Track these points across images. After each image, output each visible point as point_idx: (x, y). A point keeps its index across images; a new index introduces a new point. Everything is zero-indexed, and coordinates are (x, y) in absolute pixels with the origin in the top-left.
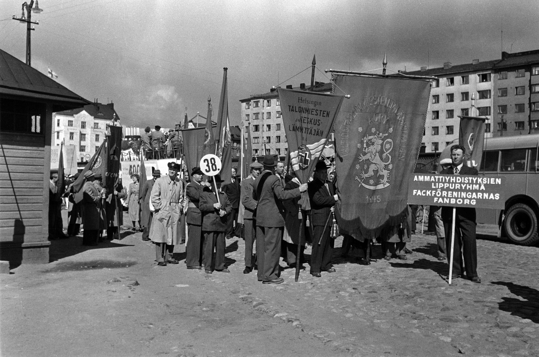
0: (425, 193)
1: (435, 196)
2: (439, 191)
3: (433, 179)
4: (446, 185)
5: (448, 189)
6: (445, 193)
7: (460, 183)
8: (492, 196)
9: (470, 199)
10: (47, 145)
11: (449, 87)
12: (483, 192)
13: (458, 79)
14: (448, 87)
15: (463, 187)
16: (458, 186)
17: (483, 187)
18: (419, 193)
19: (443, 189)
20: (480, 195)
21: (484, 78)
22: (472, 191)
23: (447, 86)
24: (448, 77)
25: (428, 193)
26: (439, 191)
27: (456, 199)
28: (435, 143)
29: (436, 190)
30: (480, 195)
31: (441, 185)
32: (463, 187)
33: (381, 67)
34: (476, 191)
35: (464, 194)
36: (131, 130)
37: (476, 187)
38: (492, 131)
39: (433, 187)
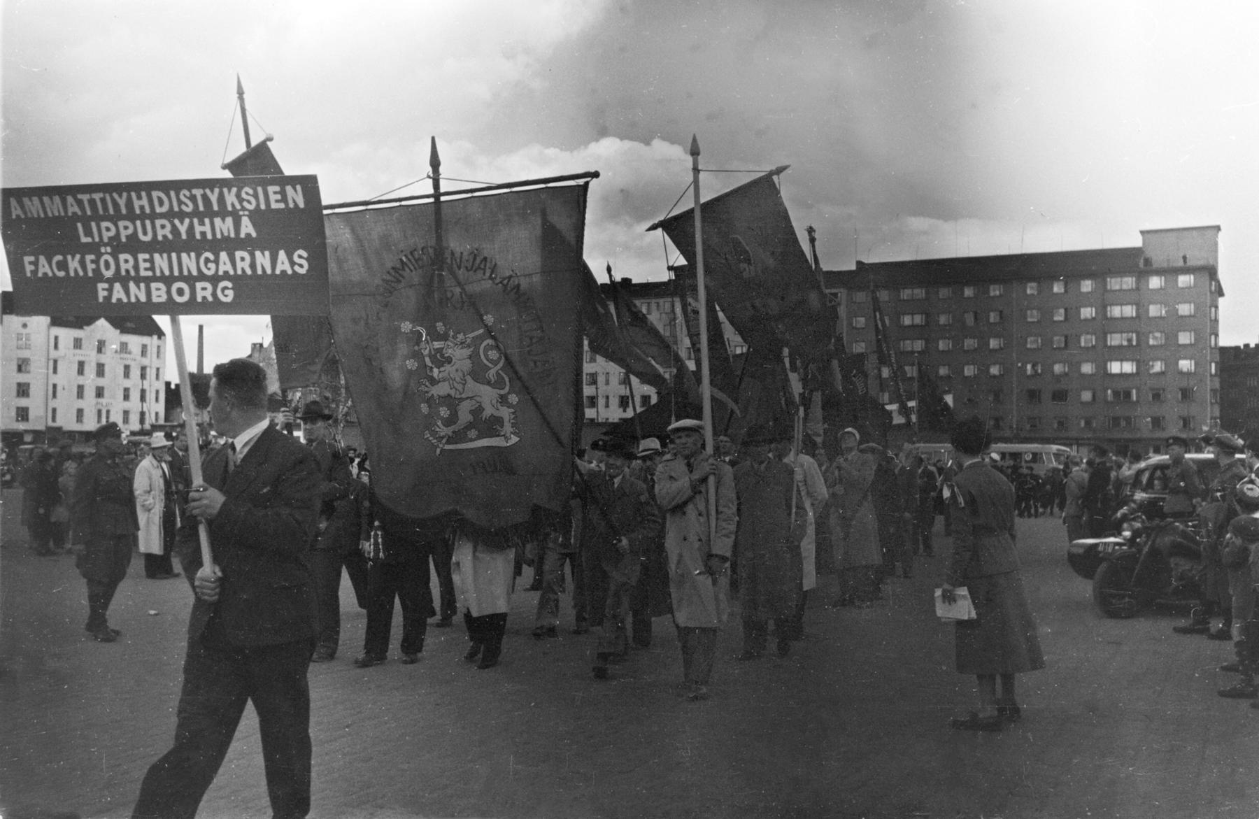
0: (63, 266)
1: (98, 277)
5: (133, 245)
8: (283, 264)
12: (248, 244)
17: (247, 228)
22: (155, 246)
25: (74, 264)
27: (168, 280)
29: (94, 248)
31: (107, 230)
34: (231, 244)
35: (189, 262)
37: (225, 227)
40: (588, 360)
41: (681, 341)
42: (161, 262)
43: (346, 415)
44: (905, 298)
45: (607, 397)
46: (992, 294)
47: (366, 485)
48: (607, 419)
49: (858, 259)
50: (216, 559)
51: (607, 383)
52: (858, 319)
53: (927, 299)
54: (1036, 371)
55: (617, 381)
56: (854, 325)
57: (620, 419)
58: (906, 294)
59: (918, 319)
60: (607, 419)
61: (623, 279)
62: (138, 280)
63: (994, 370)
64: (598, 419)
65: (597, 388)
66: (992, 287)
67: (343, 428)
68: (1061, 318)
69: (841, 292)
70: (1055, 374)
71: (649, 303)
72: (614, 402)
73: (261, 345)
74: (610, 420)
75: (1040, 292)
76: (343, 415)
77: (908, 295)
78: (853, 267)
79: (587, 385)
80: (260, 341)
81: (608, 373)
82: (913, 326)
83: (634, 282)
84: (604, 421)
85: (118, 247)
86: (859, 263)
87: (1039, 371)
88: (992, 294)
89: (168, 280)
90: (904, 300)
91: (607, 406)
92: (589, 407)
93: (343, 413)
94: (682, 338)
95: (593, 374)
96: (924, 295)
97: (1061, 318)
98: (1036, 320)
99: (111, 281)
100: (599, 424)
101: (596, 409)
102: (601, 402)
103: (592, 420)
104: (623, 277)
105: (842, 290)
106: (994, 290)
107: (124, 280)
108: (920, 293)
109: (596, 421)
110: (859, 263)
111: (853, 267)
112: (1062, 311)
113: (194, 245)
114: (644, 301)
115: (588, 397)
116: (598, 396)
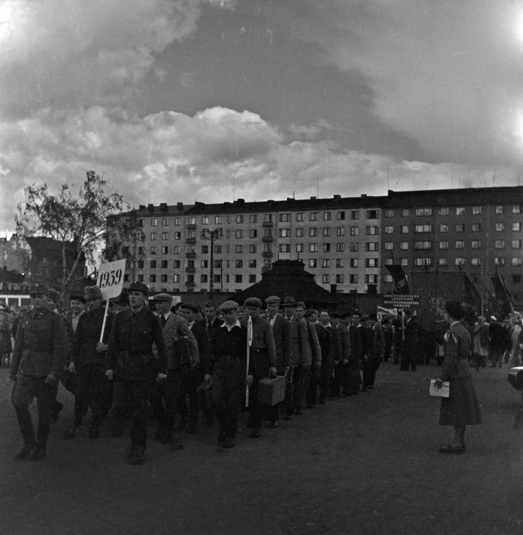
0: (389, 302)
1: (393, 303)
2: (395, 301)
3: (391, 296)
4: (398, 299)
5: (398, 300)
6: (397, 302)
7: (403, 297)
8: (416, 303)
9: (408, 305)
10: (176, 206)
11: (341, 221)
12: (412, 301)
13: (348, 213)
14: (339, 221)
15: (404, 299)
16: (402, 299)
17: (412, 299)
18: (387, 302)
19: (396, 300)
20: (411, 303)
21: (373, 215)
22: (401, 301)
23: (338, 220)
24: (338, 211)
25: (391, 302)
26: (395, 301)
27: (402, 304)
28: (255, 265)
29: (394, 300)
30: (411, 303)
31: (395, 299)
32: (404, 299)
33: (10, 230)
34: (410, 301)
35: (405, 303)
36: (178, 223)
37: (409, 299)
38: (380, 266)
39: (392, 299)
40: (216, 252)
41: (276, 240)
42: (401, 302)
43: (66, 286)
44: (419, 215)
45: (228, 276)
46: (474, 213)
47: (330, 327)
48: (228, 290)
49: (390, 189)
50: (405, 336)
51: (228, 266)
52: (389, 227)
53: (433, 215)
54: (501, 263)
55: (234, 265)
56: (386, 231)
57: (236, 290)
58: (419, 212)
59: (427, 228)
60: (228, 290)
61: (239, 200)
62: (398, 304)
63: (475, 262)
64: (222, 290)
65: (222, 270)
66: (474, 208)
67: (65, 294)
68: (518, 229)
69: (378, 211)
70: (513, 264)
71: (255, 216)
72: (232, 279)
73: (5, 239)
74: (230, 291)
75: (504, 212)
76: (65, 286)
77: (420, 213)
78: (386, 194)
79: (215, 267)
80: (5, 237)
81: (228, 260)
82: (424, 233)
83: (246, 201)
84: (226, 291)
85: (396, 300)
86: (390, 192)
87: (503, 263)
88: (474, 213)
89: (402, 304)
90: (418, 216)
91: (228, 281)
92: (216, 282)
93: (65, 285)
94: (276, 238)
95: (219, 261)
96: (431, 214)
97: (518, 229)
98: (501, 230)
99: (395, 304)
100: (224, 293)
101: (220, 283)
102: (224, 279)
103: (218, 290)
104: (239, 198)
105: (379, 209)
106: (476, 210)
107: (397, 304)
108: (428, 211)
109: (221, 291)
110: (390, 192)
111: (386, 194)
112: (518, 225)
113: (405, 301)
114: (252, 214)
115: (216, 275)
116: (222, 275)
